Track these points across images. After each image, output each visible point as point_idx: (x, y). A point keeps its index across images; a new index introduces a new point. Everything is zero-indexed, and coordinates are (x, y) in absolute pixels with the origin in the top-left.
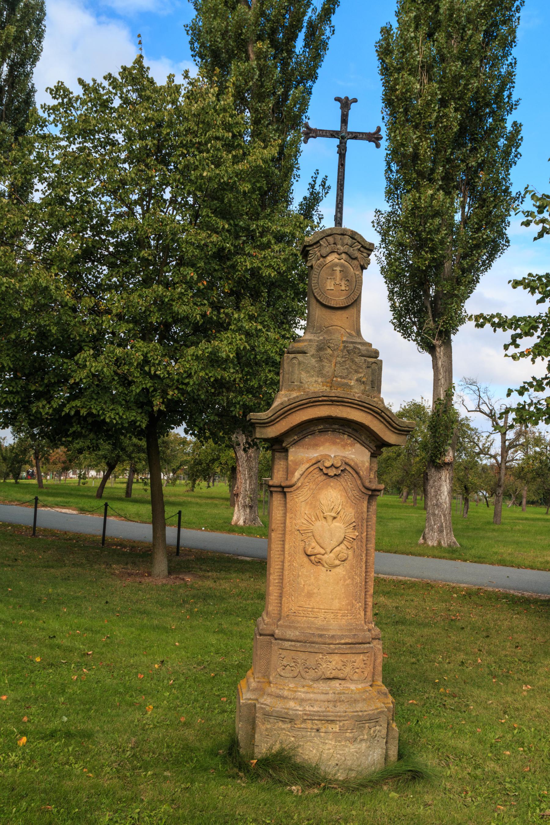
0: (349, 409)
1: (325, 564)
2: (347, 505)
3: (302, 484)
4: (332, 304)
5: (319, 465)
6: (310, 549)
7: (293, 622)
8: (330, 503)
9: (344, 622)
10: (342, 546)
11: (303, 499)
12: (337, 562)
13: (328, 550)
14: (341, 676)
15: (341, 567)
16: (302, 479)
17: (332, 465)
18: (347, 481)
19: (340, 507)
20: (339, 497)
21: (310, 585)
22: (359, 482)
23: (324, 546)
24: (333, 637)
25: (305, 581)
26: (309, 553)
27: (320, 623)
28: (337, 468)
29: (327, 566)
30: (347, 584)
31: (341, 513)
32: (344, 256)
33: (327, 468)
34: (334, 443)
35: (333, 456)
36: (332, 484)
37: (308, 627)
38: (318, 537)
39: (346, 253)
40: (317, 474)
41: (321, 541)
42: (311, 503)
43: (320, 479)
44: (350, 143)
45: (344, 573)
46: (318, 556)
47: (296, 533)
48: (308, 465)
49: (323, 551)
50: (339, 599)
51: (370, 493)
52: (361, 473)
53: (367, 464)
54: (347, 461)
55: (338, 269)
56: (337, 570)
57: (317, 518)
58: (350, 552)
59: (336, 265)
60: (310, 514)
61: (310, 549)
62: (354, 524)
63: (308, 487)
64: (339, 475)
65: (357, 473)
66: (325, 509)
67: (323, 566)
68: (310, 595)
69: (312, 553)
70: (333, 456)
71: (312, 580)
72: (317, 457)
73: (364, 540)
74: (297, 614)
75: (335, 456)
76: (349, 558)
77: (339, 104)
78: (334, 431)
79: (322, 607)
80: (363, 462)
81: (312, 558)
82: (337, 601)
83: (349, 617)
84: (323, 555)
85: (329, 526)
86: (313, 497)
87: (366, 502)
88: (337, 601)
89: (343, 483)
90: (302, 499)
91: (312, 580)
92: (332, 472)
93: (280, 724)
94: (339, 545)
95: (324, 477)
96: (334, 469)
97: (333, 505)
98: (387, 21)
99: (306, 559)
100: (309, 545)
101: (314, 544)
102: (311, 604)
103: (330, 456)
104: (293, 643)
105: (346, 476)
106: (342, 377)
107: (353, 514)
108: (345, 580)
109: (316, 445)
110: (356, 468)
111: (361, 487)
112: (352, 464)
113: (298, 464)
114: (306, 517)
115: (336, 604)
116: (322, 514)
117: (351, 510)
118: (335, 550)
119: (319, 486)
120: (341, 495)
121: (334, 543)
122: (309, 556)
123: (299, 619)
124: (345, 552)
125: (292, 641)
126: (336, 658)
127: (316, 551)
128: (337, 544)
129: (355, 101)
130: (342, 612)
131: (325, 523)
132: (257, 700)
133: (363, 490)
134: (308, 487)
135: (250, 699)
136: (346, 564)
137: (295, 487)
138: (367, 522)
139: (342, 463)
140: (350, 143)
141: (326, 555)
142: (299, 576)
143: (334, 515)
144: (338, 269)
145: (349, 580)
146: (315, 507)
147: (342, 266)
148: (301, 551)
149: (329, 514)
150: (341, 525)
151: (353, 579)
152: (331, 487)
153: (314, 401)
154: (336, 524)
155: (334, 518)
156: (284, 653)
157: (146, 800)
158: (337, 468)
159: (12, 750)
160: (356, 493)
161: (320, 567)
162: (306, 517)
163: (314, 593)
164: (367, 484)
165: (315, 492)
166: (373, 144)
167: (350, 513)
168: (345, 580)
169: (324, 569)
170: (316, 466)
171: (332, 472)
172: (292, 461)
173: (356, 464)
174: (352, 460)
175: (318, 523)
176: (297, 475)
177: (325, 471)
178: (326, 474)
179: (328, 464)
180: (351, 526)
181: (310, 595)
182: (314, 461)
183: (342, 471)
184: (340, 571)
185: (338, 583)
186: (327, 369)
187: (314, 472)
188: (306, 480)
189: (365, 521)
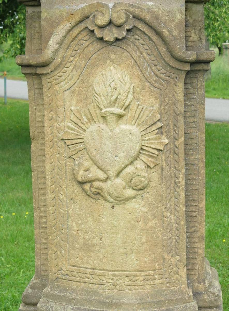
1: (108, 197)
2: (144, 92)
3: (62, 60)
5: (89, 24)
6: (81, 172)
7: (65, 289)
8: (109, 90)
9: (148, 289)
10: (139, 165)
11: (67, 86)
12: (129, 192)
13: (112, 173)
15: (139, 200)
16: (62, 51)
17: (110, 22)
18: (141, 49)
19: (130, 96)
20: (127, 79)
21: (86, 232)
22: (163, 50)
23: (104, 165)
25: (79, 225)
26: (80, 179)
27: (107, 292)
28: (119, 26)
29: (112, 200)
30: (152, 228)
31: (133, 107)
33: (101, 27)
35: (111, 5)
36: (113, 56)
37: (87, 300)
40: (85, 40)
41: (98, 158)
42: (80, 93)
43: (91, 48)
45: (145, 209)
46: (96, 184)
47: (60, 144)
48: (68, 25)
49: (102, 175)
50: (137, 253)
51: (187, 67)
52: (166, 33)
53: (180, 17)
54: (137, 12)
56: (132, 205)
57: (91, 119)
58: (155, 175)
60: (78, 111)
61: (81, 172)
62: (160, 124)
63: (73, 64)
64: (124, 38)
65: (159, 34)
66: (102, 101)
67: (106, 200)
68: (88, 248)
69: (84, 179)
70: (111, 5)
71: (90, 223)
72: (83, 9)
73: (181, 151)
74: (71, 278)
75: (114, 6)
76: (152, 184)
79: (108, 268)
80: (171, 13)
81: (87, 186)
82: (133, 256)
83: (157, 282)
84: (104, 181)
85: (111, 131)
86: (83, 82)
87: (181, 85)
88: (133, 256)
89: (133, 53)
90: (65, 85)
91: (90, 223)
92: (110, 35)
94: (131, 163)
95: (97, 45)
96: (114, 30)
97: (117, 93)
99: (77, 189)
100: (80, 165)
101: (87, 164)
102: (91, 262)
103: (107, 5)
105: (136, 38)
107: (156, 107)
108: (146, 221)
110: (154, 23)
111: (168, 58)
112: (148, 17)
113: (54, 24)
114: (72, 117)
115: (133, 262)
116: (98, 112)
117: (152, 99)
118: (124, 172)
119: (91, 62)
120: (131, 76)
121: (121, 160)
122: (81, 183)
123: (74, 285)
124: (143, 174)
127: (90, 175)
128: (126, 162)
130: (143, 274)
131: (103, 126)
133: (173, 63)
134: (73, 64)
136: (149, 195)
137: (52, 66)
138: (185, 118)
139: (128, 16)
141: (109, 182)
142: (68, 217)
143: (117, 110)
145: (155, 221)
146: (86, 99)
149: (108, 109)
150: (134, 129)
151: (162, 218)
152: (112, 61)
154: (124, 127)
155: (120, 117)
158: (119, 26)
159: (180, 239)
160: (159, 69)
161: (102, 202)
162: (72, 117)
163: (94, 245)
164: (181, 52)
165: (85, 72)
167: (151, 106)
168: (146, 221)
170: (82, 26)
171: (110, 35)
172: (46, 19)
173: (157, 17)
174: (149, 10)
175: (93, 128)
176: (52, 44)
177: (98, 33)
178: (101, 39)
179: (102, 20)
180: (154, 128)
182: (77, 18)
183: (128, 30)
184: (138, 206)
185: (134, 227)
187: (80, 37)
188: (69, 52)
189: (181, 118)
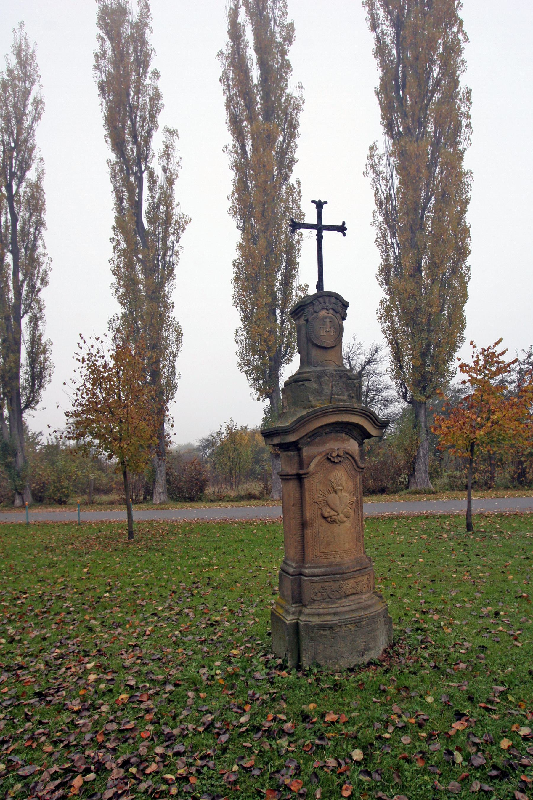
0: (350, 415)
4: (326, 345)
14: (355, 592)
24: (348, 568)
26: (326, 516)
27: (338, 560)
32: (331, 311)
34: (337, 440)
38: (332, 505)
39: (333, 309)
41: (334, 507)
44: (325, 233)
55: (328, 320)
59: (326, 318)
68: (328, 544)
77: (314, 205)
78: (337, 432)
81: (329, 519)
90: (316, 481)
93: (322, 632)
95: (331, 464)
98: (470, 87)
99: (323, 521)
104: (321, 578)
106: (338, 395)
108: (351, 530)
109: (324, 443)
125: (319, 576)
126: (352, 581)
129: (326, 203)
132: (298, 619)
135: (293, 619)
140: (325, 233)
144: (328, 320)
147: (331, 318)
148: (319, 516)
153: (325, 413)
156: (315, 585)
157: (494, 760)
161: (335, 524)
166: (341, 234)
169: (337, 525)
176: (312, 465)
181: (328, 544)
186: (326, 390)
